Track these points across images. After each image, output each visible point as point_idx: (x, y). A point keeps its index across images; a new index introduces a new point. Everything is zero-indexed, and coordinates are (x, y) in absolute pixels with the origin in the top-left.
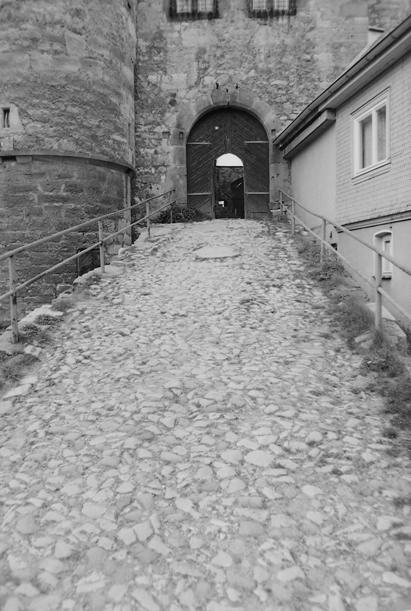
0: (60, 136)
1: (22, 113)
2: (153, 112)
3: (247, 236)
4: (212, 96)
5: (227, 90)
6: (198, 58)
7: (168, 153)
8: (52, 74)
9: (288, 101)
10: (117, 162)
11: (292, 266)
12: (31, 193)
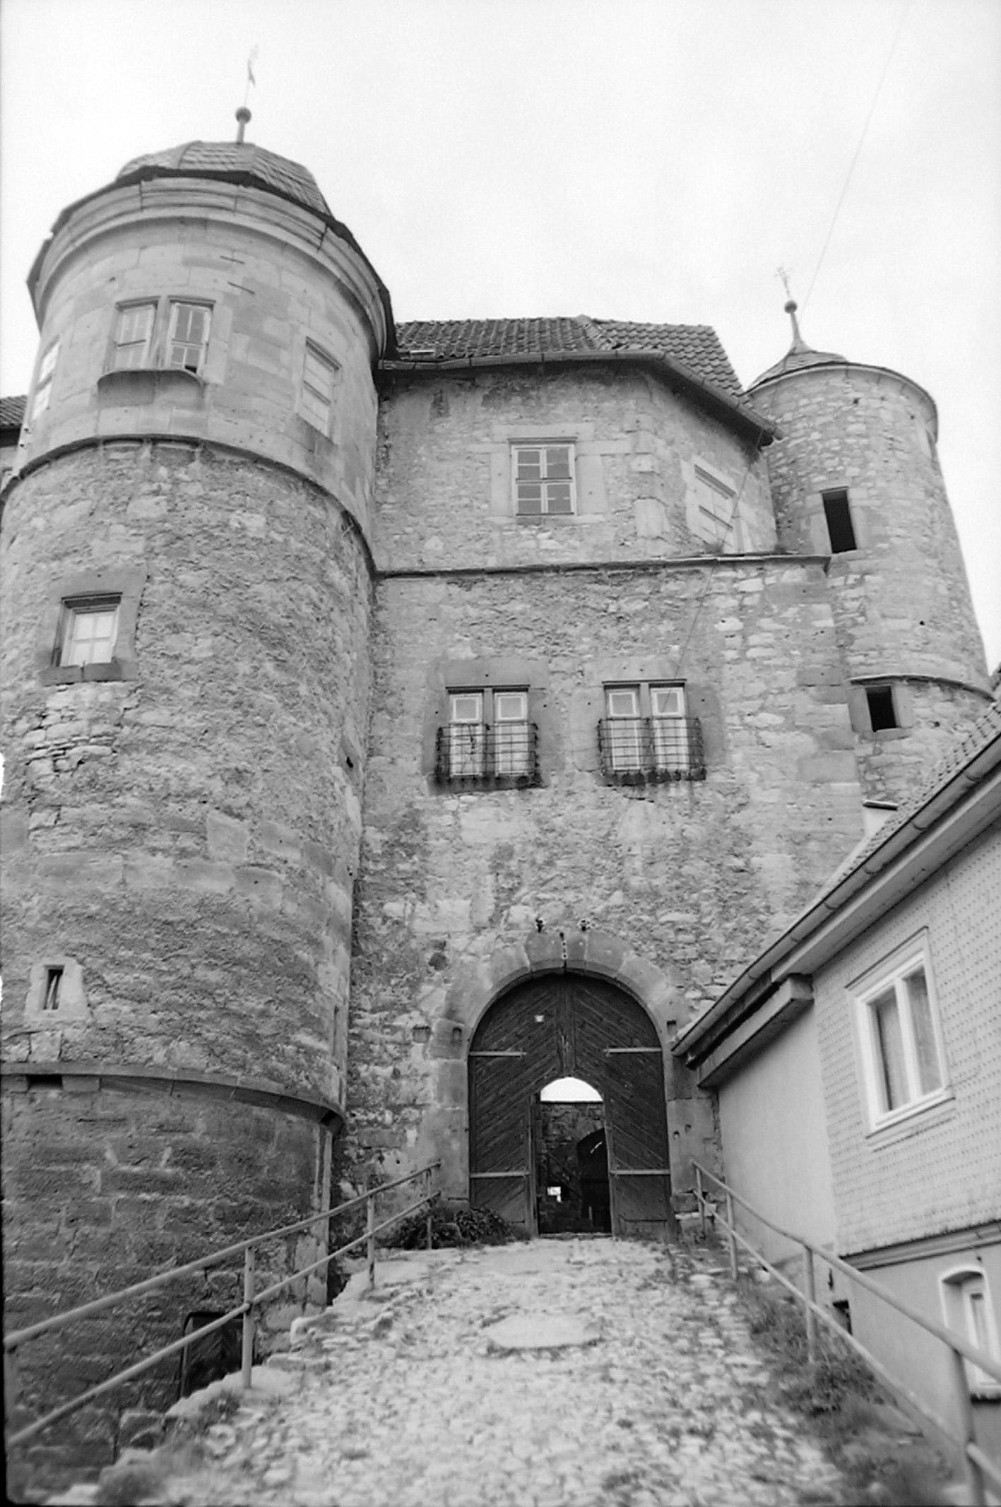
0: (171, 1033)
1: (91, 979)
2: (393, 982)
3: (619, 1286)
4: (527, 948)
5: (562, 935)
6: (496, 868)
7: (426, 1075)
8: (170, 897)
9: (700, 956)
10: (301, 1096)
11: (736, 1371)
12: (86, 1166)
